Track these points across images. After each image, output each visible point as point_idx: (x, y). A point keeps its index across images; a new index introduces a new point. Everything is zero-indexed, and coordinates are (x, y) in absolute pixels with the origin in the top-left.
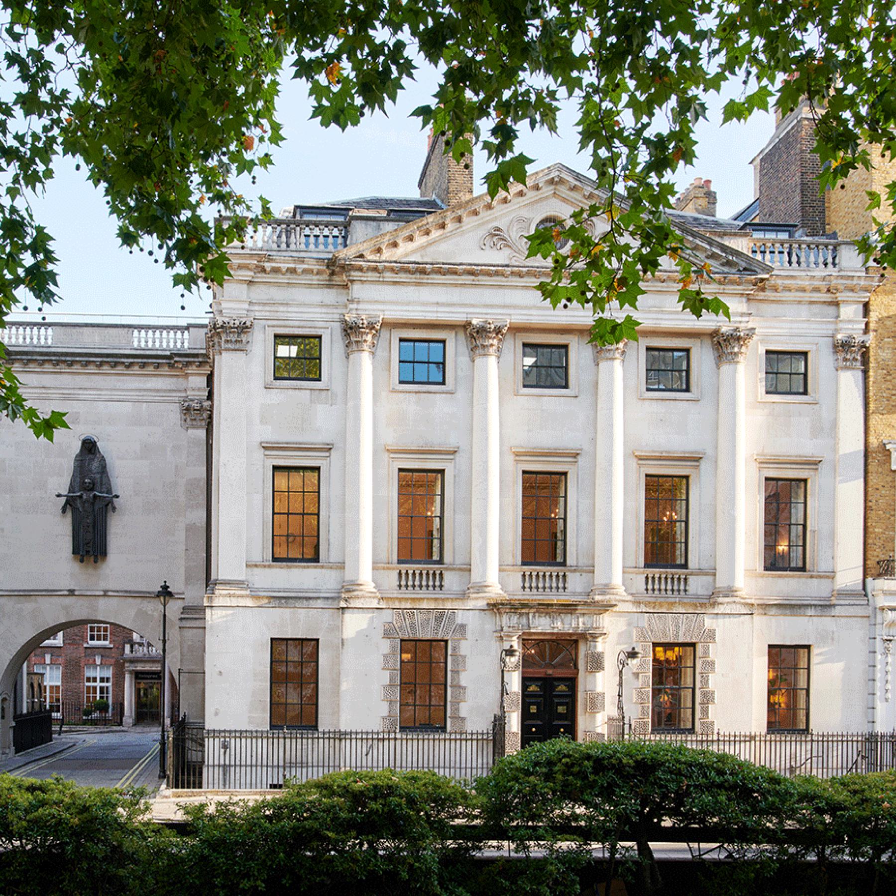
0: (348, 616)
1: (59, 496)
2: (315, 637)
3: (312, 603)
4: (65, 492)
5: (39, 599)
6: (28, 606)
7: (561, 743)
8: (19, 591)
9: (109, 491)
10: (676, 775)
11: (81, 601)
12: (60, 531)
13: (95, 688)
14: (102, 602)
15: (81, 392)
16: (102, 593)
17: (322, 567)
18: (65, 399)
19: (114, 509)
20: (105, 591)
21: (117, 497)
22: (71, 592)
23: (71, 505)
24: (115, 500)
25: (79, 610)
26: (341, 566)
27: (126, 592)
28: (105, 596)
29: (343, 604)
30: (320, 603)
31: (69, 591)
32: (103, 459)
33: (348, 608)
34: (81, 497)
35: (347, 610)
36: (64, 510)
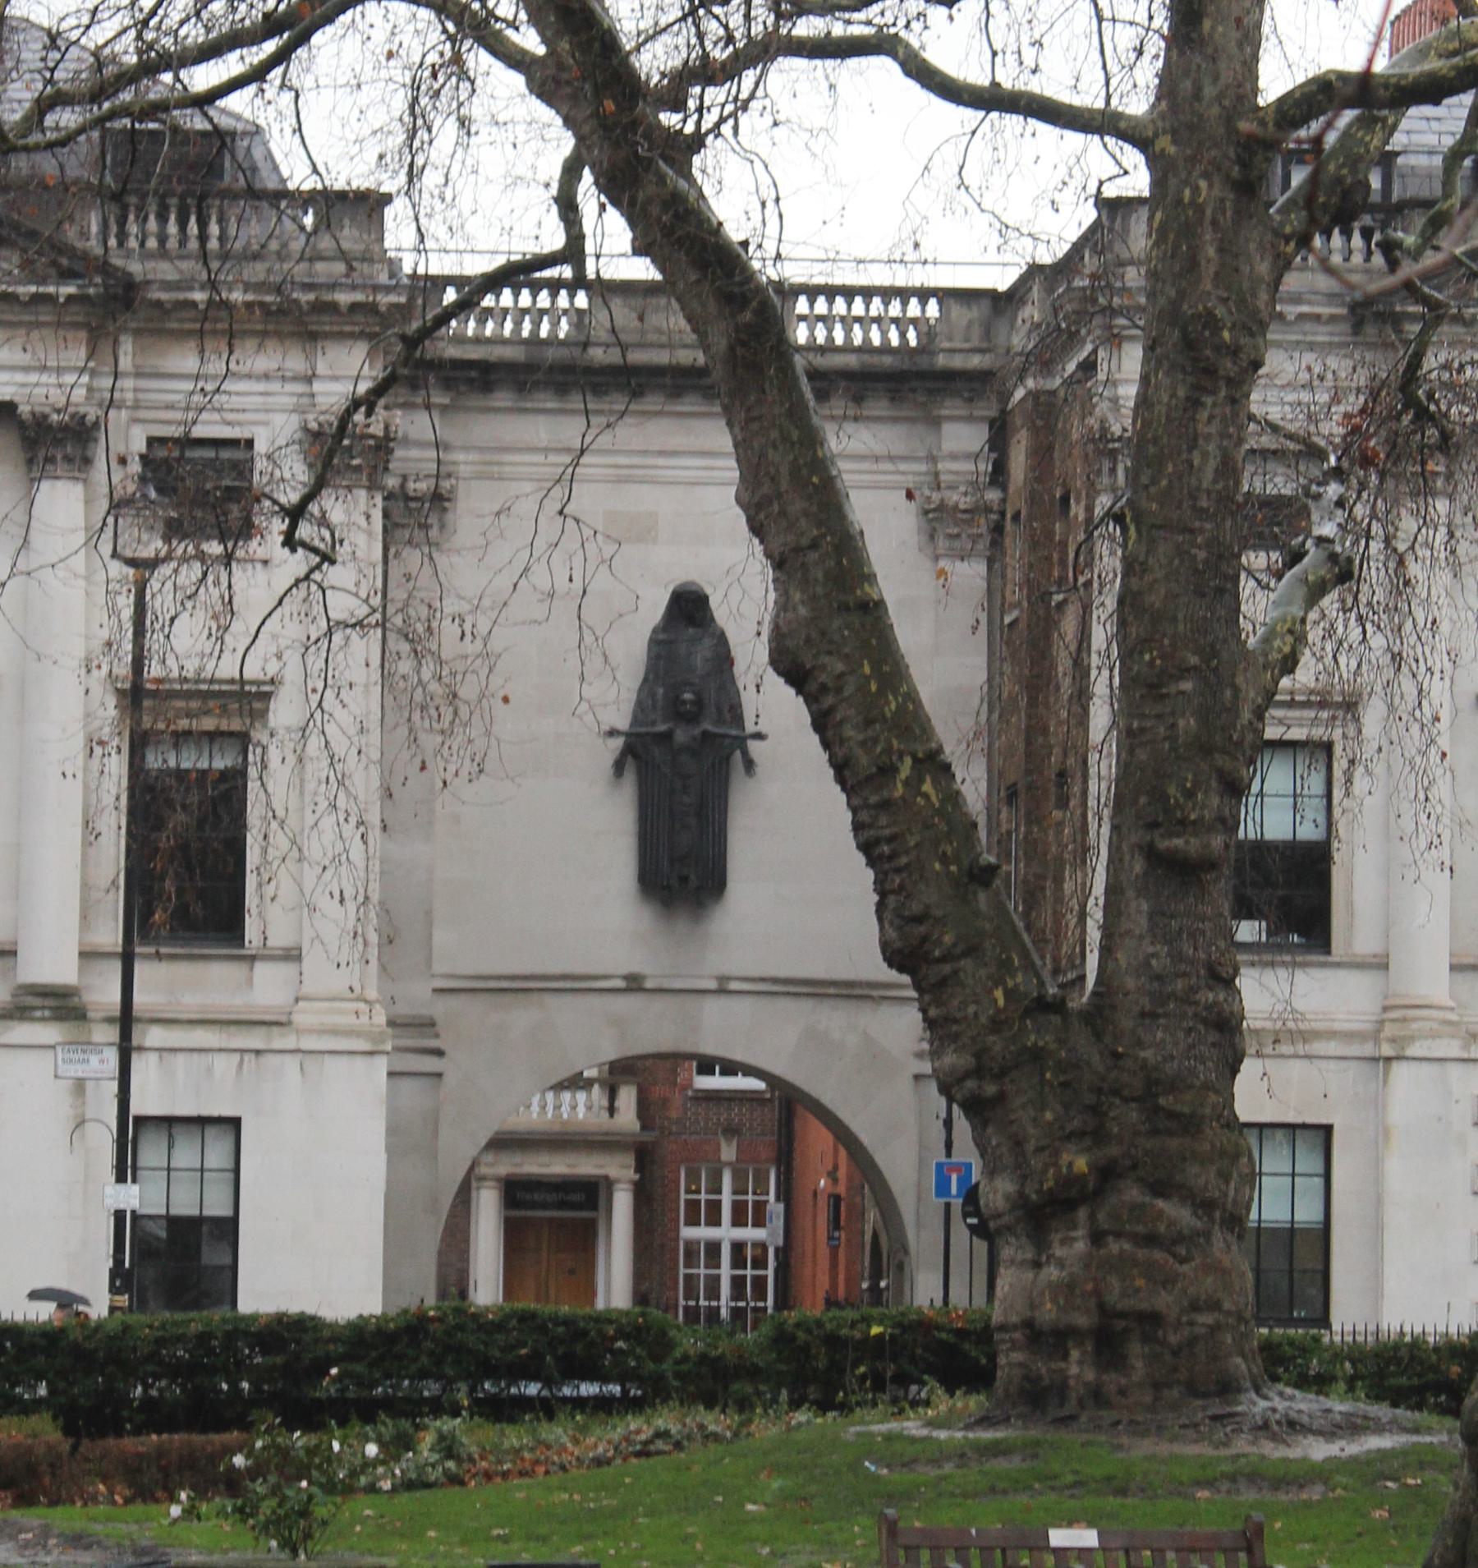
0: (1400, 1070)
1: (612, 733)
2: (1324, 1121)
3: (1318, 1047)
4: (623, 723)
5: (550, 1000)
6: (522, 1017)
7: (217, 1314)
8: (499, 978)
9: (738, 718)
10: (1161, 439)
11: (659, 1005)
12: (603, 828)
13: (738, 1220)
14: (713, 1007)
15: (661, 461)
16: (713, 985)
17: (1338, 965)
18: (620, 480)
19: (749, 765)
20: (723, 979)
21: (759, 736)
22: (634, 984)
23: (636, 756)
24: (754, 746)
25: (652, 1029)
26: (1380, 964)
27: (775, 981)
28: (722, 991)
29: (1387, 1050)
30: (1332, 1047)
31: (626, 978)
32: (722, 639)
33: (1398, 1058)
34: (667, 736)
35: (1395, 1065)
36: (619, 767)
